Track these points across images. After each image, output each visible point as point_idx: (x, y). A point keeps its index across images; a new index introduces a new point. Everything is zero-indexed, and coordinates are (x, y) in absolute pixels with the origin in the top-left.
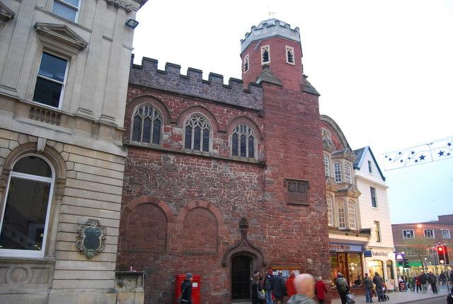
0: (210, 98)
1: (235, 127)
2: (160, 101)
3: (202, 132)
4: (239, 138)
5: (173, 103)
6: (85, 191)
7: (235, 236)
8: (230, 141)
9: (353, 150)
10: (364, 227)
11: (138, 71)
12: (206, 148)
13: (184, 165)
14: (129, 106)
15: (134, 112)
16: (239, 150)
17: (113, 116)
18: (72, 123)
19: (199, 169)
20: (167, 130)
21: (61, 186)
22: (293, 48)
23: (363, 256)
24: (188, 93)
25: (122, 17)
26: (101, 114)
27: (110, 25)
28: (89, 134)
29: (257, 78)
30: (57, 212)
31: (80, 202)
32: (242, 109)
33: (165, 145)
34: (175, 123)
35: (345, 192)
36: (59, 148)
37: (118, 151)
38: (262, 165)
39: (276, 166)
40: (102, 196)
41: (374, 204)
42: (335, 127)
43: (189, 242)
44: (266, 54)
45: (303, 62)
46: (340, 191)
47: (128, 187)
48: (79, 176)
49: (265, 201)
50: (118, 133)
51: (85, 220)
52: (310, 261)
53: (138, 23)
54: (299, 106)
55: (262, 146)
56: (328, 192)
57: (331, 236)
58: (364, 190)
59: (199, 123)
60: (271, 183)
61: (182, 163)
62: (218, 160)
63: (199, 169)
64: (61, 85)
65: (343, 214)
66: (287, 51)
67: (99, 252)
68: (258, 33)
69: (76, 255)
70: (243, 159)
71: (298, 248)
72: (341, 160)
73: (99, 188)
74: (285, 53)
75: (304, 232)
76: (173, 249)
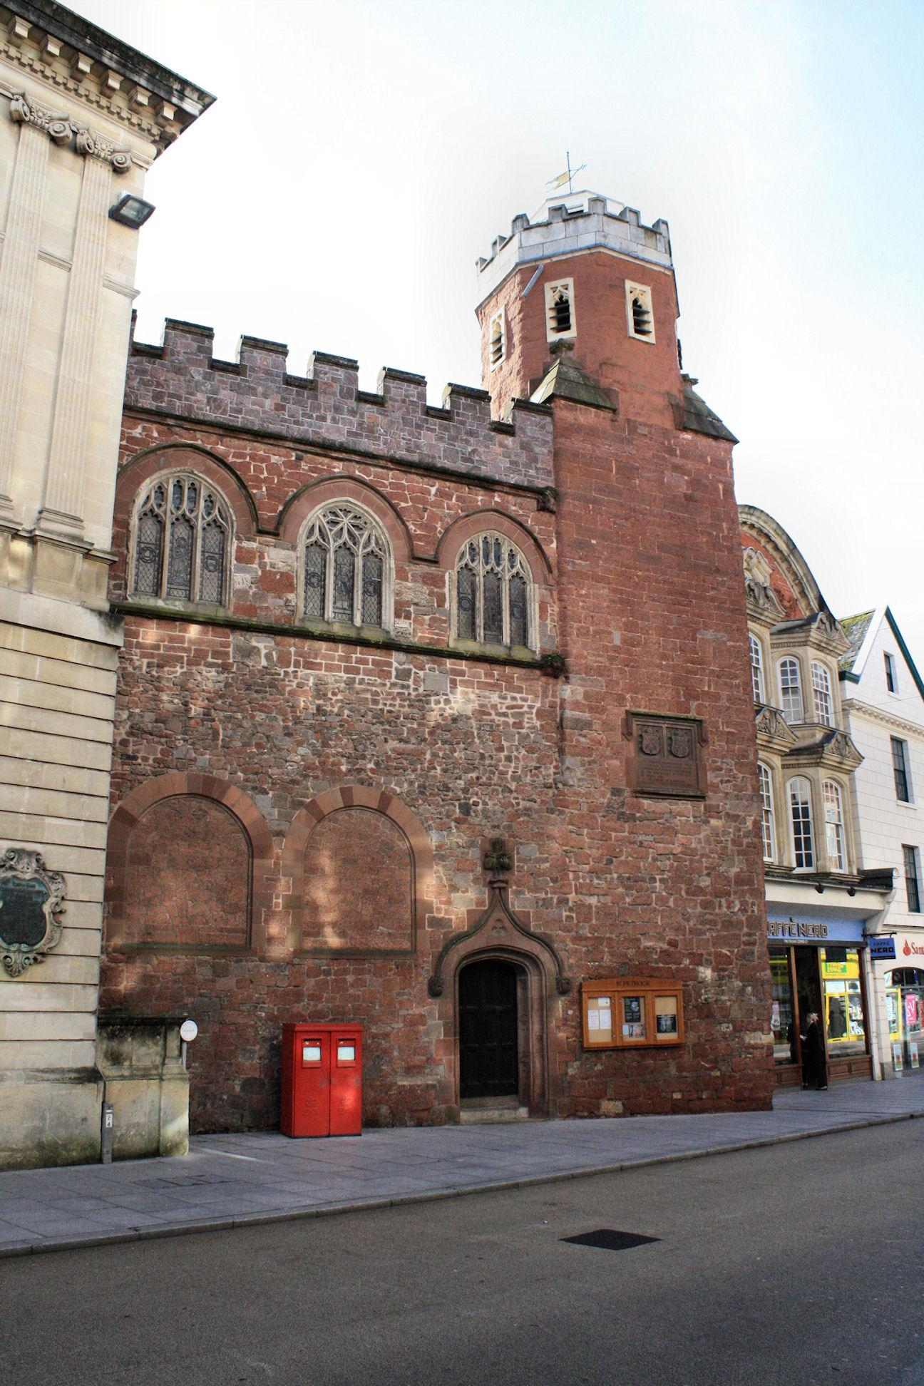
1: (464, 546)
2: (221, 461)
9: (837, 616)
10: (871, 864)
11: (149, 366)
14: (127, 478)
15: (140, 500)
20: (245, 557)
22: (648, 289)
23: (867, 955)
24: (311, 436)
26: (38, 507)
32: (488, 484)
34: (276, 531)
35: (813, 753)
37: (93, 628)
38: (553, 667)
39: (599, 671)
40: (49, 776)
41: (904, 792)
42: (783, 546)
44: (562, 308)
45: (681, 333)
46: (796, 752)
47: (124, 743)
50: (81, 564)
52: (707, 973)
53: (152, 209)
55: (554, 609)
56: (762, 754)
57: (775, 894)
60: (581, 725)
61: (297, 664)
65: (804, 821)
68: (535, 237)
71: (670, 935)
72: (800, 651)
74: (624, 304)
75: (690, 882)
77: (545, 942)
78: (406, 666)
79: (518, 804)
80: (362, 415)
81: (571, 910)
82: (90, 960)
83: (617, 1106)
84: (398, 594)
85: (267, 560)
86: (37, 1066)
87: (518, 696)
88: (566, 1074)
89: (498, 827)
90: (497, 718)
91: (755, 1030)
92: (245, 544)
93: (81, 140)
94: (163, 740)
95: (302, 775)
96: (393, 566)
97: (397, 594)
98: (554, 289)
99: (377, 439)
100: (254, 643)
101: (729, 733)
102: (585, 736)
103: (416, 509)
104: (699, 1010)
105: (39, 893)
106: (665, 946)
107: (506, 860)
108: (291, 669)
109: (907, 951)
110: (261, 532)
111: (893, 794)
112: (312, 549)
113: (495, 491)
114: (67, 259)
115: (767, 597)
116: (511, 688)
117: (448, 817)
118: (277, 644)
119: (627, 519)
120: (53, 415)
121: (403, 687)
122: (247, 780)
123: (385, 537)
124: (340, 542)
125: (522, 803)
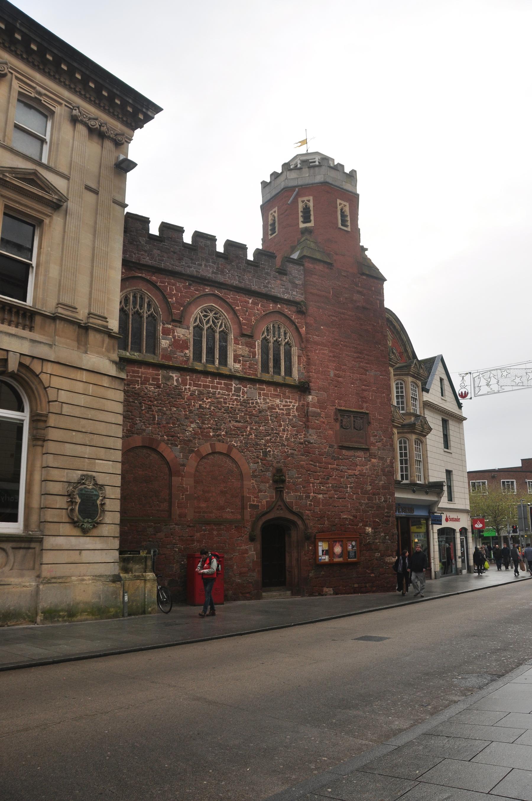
0: (229, 281)
1: (264, 328)
2: (154, 284)
3: (217, 336)
4: (271, 345)
5: (175, 289)
6: (74, 433)
7: (265, 496)
8: (258, 350)
10: (432, 480)
12: (224, 361)
13: (193, 388)
16: (271, 364)
17: (106, 315)
18: (50, 327)
19: (214, 394)
20: (166, 332)
21: (41, 425)
22: (347, 204)
25: (111, 155)
26: (87, 311)
27: (93, 168)
28: (75, 344)
29: (293, 250)
30: (38, 464)
31: (69, 449)
32: (275, 299)
33: (167, 357)
34: (179, 321)
36: (36, 367)
37: (113, 371)
38: (303, 388)
40: (97, 440)
41: (447, 445)
43: (203, 505)
44: (306, 211)
48: (66, 410)
49: (309, 443)
51: (75, 476)
52: (369, 530)
54: (356, 297)
55: (304, 359)
58: (434, 421)
59: (213, 322)
61: (190, 385)
62: (242, 380)
63: (214, 394)
64: (28, 266)
66: (339, 208)
67: (98, 523)
68: (293, 175)
69: (67, 528)
70: (278, 379)
72: (405, 378)
73: (89, 426)
74: (336, 212)
76: (180, 516)
77: (299, 515)
78: (239, 386)
79: (288, 451)
80: (218, 264)
81: (311, 501)
82: (115, 526)
83: (330, 590)
84: (235, 351)
85: (176, 334)
86: (96, 574)
87: (288, 400)
88: (309, 575)
89: (279, 462)
90: (279, 411)
91: (389, 556)
92: (166, 326)
93: (104, 129)
94: (130, 421)
95: (193, 437)
96: (233, 338)
97: (234, 351)
98: (303, 202)
99: (225, 275)
100: (171, 374)
101: (380, 419)
102: (317, 420)
103: (243, 310)
104: (365, 546)
105: (95, 495)
106: (352, 518)
107: (284, 478)
108: (188, 387)
109: (447, 520)
110: (174, 321)
111: (442, 446)
112: (196, 329)
113: (278, 302)
114: (97, 189)
115: (393, 353)
116: (285, 397)
117: (258, 457)
118: (181, 375)
119: (337, 317)
120: (93, 266)
121: (237, 396)
122: (168, 440)
123: (230, 323)
124: (209, 325)
125: (290, 451)
